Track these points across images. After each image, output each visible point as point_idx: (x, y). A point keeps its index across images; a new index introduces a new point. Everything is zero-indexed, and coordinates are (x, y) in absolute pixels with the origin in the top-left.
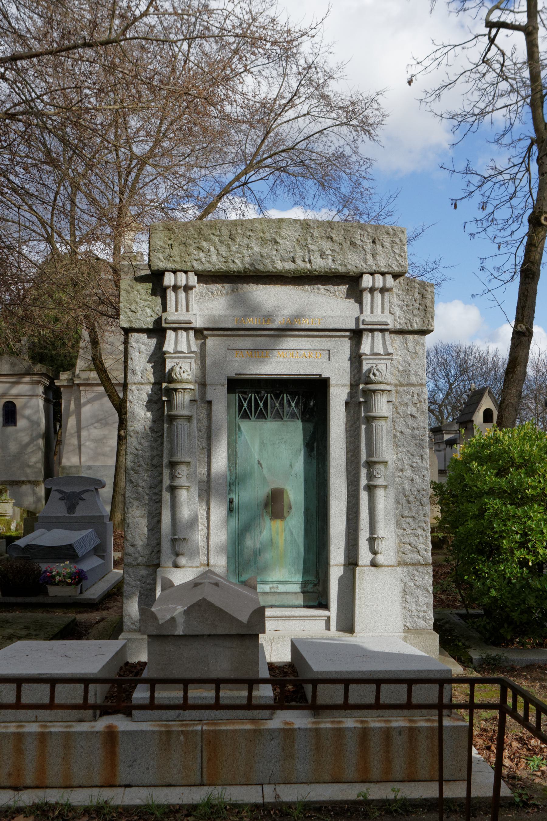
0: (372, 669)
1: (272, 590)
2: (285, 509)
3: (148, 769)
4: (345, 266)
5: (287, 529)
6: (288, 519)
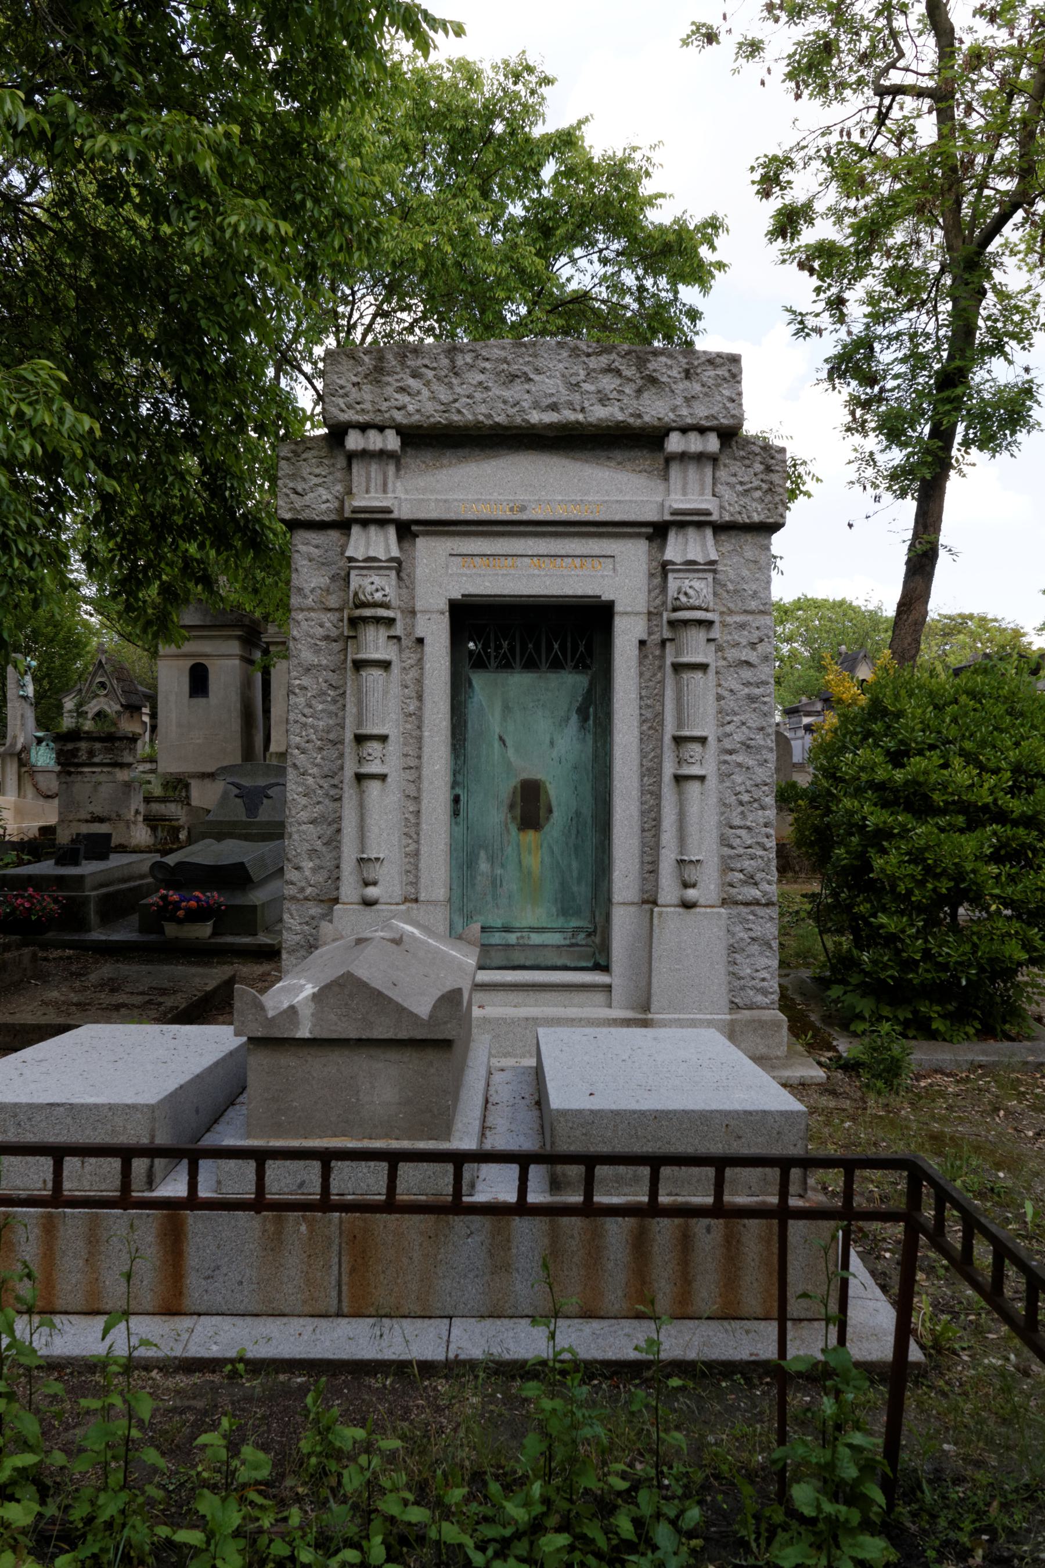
0: (659, 1107)
2: (542, 813)
3: (241, 1283)
4: (640, 416)
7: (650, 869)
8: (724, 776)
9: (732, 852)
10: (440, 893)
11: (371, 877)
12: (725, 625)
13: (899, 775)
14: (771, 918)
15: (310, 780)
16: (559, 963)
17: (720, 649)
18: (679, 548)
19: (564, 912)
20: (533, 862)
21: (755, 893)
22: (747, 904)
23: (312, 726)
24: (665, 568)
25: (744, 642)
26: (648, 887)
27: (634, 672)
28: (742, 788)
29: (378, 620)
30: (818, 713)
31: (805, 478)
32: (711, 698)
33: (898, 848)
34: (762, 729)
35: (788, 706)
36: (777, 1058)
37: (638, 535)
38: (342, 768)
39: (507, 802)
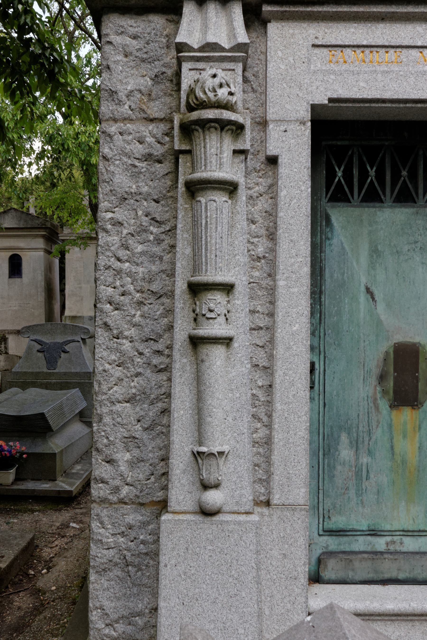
1: (392, 548)
10: (300, 493)
11: (212, 479)
15: (126, 345)
23: (129, 274)
29: (223, 125)
38: (170, 328)
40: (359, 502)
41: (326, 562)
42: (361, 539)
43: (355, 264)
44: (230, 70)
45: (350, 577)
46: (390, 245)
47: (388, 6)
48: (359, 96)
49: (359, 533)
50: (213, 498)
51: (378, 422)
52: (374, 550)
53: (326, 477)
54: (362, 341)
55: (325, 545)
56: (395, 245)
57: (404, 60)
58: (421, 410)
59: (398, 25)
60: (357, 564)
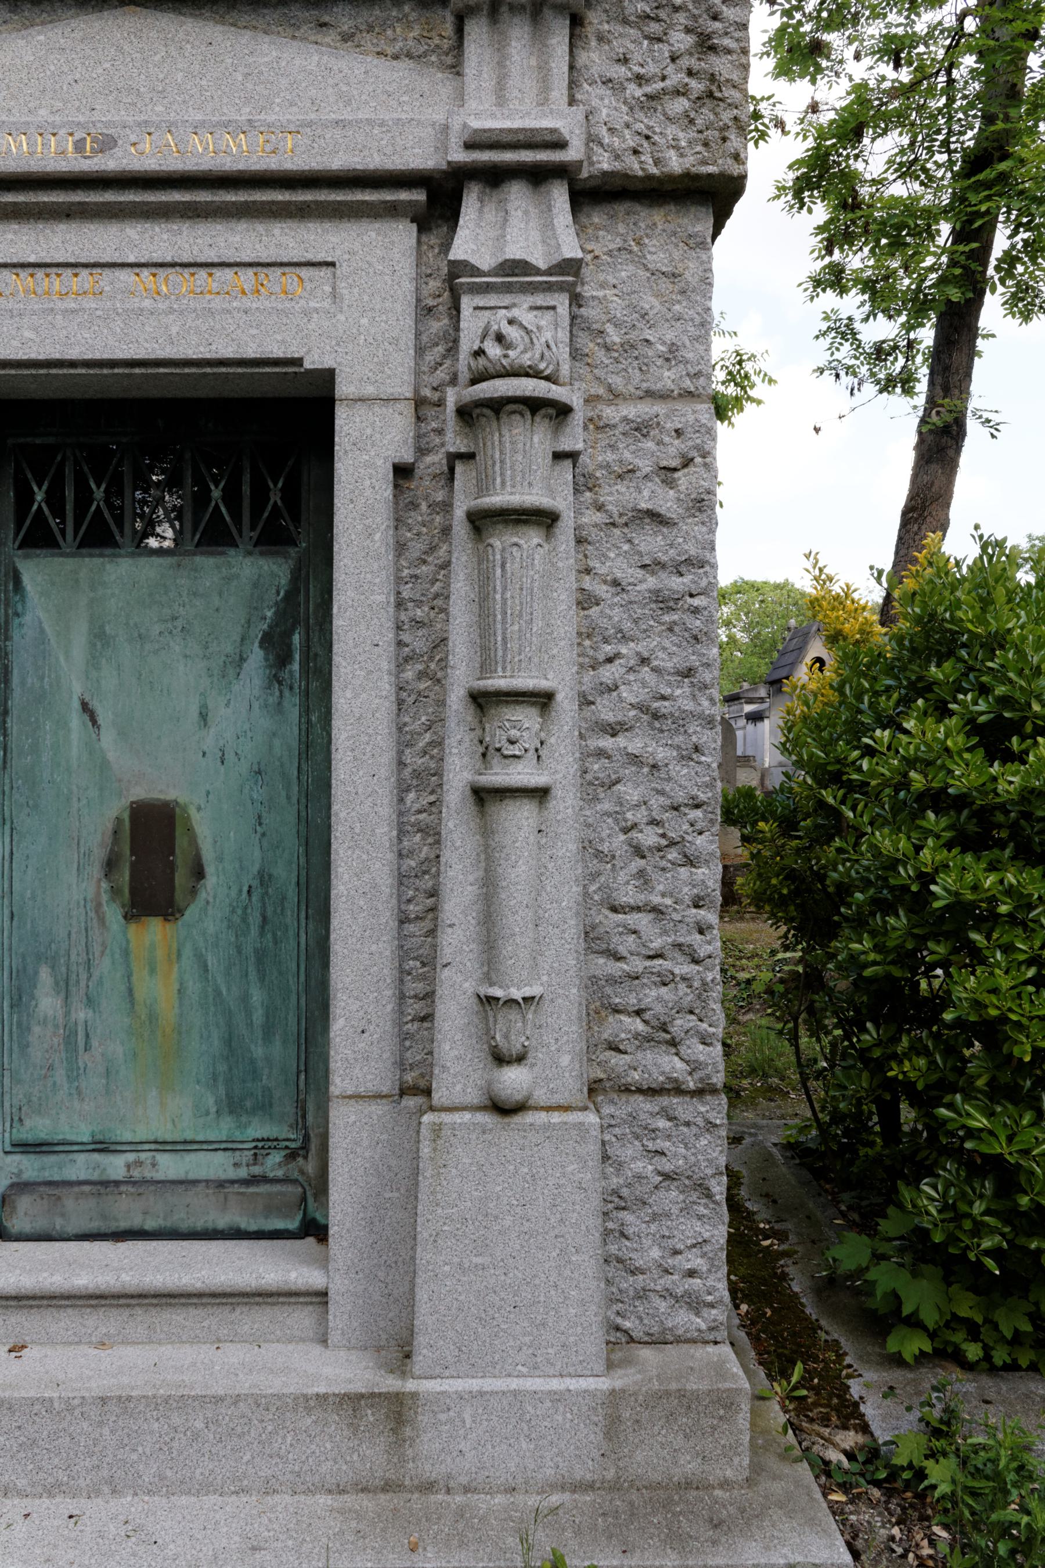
1: (136, 1174)
2: (181, 878)
5: (188, 952)
6: (191, 913)
7: (415, 1011)
8: (594, 788)
9: (615, 968)
12: (597, 425)
13: (1010, 781)
14: (710, 1126)
16: (222, 1222)
17: (584, 484)
18: (491, 232)
19: (233, 1106)
20: (159, 991)
21: (669, 1065)
22: (651, 1092)
24: (457, 281)
25: (645, 466)
26: (413, 1056)
27: (381, 538)
28: (640, 816)
30: (762, 700)
31: (754, 378)
32: (564, 598)
33: (1008, 949)
34: (688, 673)
35: (726, 693)
36: (725, 1484)
37: (392, 211)
39: (99, 855)
40: (74, 1091)
41: (14, 1202)
42: (81, 1158)
43: (62, 659)
44: (548, 308)
45: (58, 1227)
46: (127, 624)
47: (70, 193)
48: (21, 355)
49: (75, 1148)
50: (513, 1080)
51: (104, 945)
52: (104, 1178)
53: (15, 1047)
54: (75, 799)
55: (16, 1171)
56: (136, 625)
57: (107, 289)
58: (180, 923)
59: (92, 227)
60: (69, 1203)
